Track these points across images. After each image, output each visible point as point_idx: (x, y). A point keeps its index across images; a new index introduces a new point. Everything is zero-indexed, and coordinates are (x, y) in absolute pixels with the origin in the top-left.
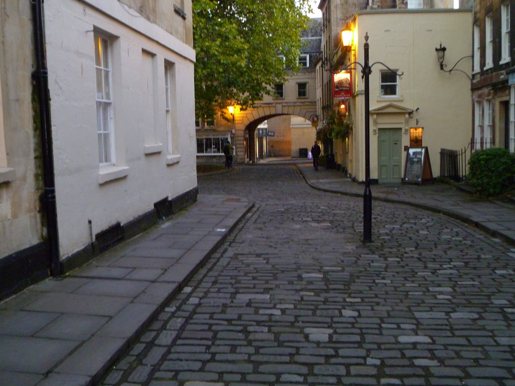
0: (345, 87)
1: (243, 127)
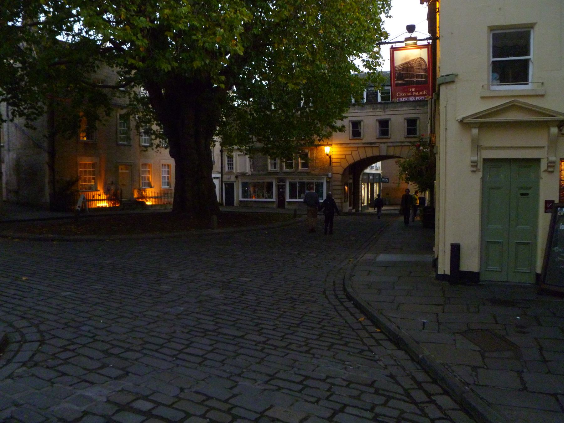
0: (417, 76)
1: (341, 170)
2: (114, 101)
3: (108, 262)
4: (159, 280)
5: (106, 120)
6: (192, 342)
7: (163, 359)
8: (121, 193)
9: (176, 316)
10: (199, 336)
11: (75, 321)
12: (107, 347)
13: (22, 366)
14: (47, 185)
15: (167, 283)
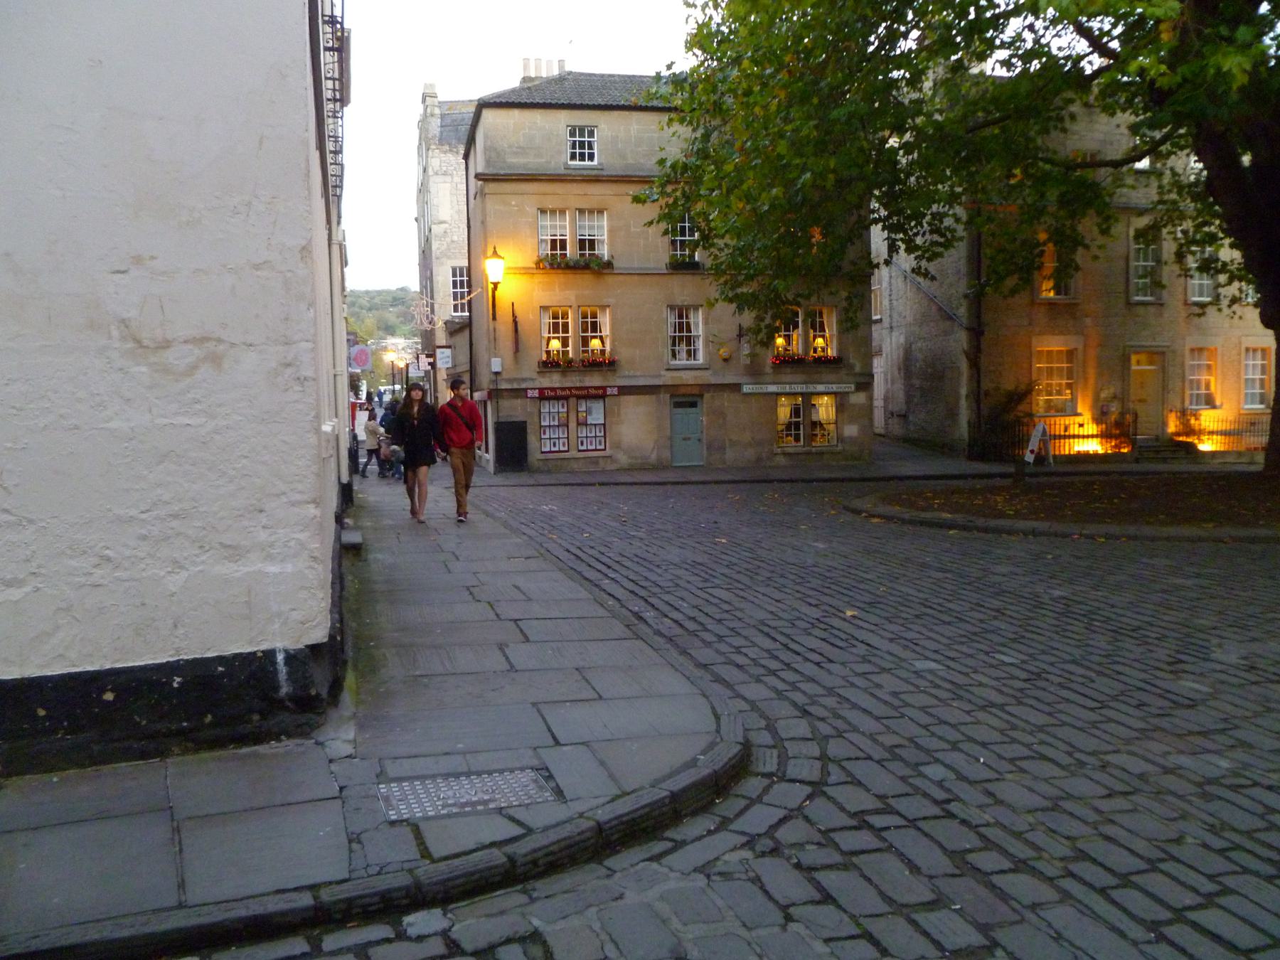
2: (1124, 200)
3: (1057, 593)
4: (1181, 661)
5: (1100, 247)
6: (1226, 891)
7: (1114, 929)
8: (1135, 421)
9: (1200, 785)
10: (1257, 874)
11: (918, 746)
12: (968, 840)
13: (743, 846)
14: (963, 403)
15: (1201, 674)
